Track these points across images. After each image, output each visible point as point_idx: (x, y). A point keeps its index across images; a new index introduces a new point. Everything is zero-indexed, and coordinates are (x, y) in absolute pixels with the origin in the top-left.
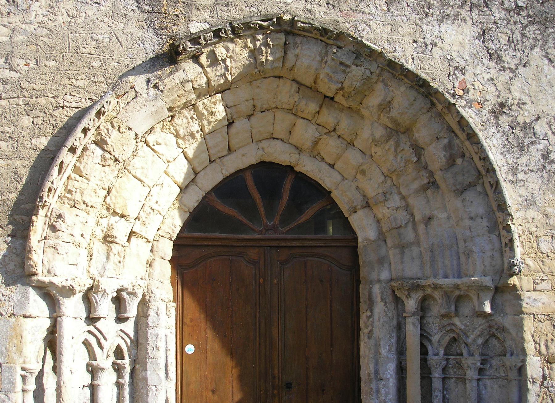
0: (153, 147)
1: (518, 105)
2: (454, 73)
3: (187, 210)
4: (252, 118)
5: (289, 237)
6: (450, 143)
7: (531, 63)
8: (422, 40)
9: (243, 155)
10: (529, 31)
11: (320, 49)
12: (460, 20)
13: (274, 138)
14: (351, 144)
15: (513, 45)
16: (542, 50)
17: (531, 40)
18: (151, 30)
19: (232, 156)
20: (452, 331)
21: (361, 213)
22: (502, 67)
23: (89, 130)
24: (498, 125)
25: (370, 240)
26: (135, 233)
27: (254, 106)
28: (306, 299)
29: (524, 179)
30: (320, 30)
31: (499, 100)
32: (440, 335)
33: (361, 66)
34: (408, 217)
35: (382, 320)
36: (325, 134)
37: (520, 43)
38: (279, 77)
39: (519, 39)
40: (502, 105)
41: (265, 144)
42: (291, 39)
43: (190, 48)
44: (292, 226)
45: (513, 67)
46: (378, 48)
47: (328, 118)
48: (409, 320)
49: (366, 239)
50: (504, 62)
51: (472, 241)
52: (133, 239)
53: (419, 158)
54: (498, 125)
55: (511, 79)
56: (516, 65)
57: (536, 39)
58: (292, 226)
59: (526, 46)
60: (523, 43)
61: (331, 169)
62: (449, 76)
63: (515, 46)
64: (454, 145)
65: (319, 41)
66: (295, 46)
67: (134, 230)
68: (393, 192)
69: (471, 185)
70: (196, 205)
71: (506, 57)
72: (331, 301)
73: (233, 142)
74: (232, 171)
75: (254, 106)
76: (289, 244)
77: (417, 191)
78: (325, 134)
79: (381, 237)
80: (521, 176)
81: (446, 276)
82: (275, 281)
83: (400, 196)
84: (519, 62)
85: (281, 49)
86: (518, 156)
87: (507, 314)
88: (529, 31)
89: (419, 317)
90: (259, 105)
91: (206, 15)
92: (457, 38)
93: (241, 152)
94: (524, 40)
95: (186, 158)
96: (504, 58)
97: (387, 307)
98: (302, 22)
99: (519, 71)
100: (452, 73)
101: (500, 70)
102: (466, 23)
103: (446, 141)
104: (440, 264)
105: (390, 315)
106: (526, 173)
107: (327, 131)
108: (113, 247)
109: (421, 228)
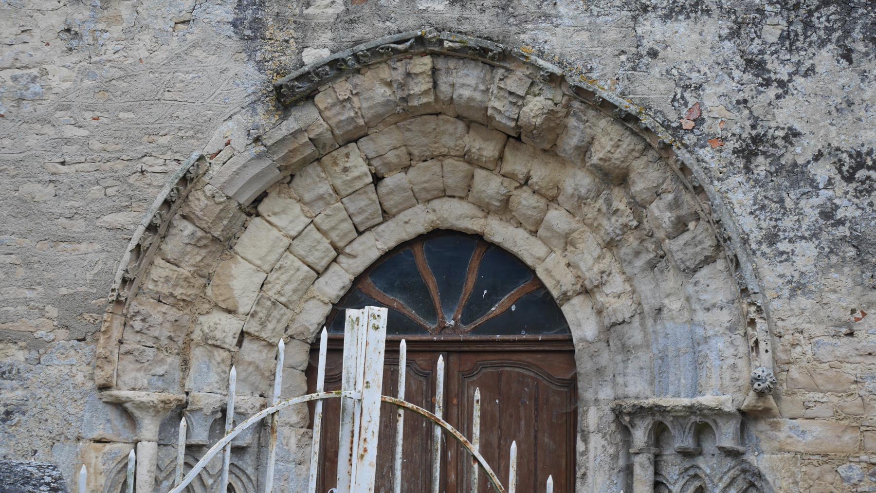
0: (268, 218)
1: (785, 138)
2: (683, 97)
3: (327, 300)
4: (411, 170)
5: (473, 338)
6: (676, 199)
7: (816, 70)
8: (634, 50)
9: (406, 223)
10: (818, 18)
11: (482, 75)
12: (699, 13)
13: (449, 196)
14: (553, 200)
15: (787, 43)
16: (840, 46)
17: (822, 33)
18: (252, 64)
19: (391, 224)
20: (696, 476)
21: (577, 301)
22: (764, 79)
23: (173, 202)
24: (748, 169)
25: (587, 341)
26: (249, 334)
27: (410, 154)
28: (500, 428)
29: (789, 250)
30: (476, 49)
31: (754, 133)
32: (682, 483)
33: (539, 95)
34: (634, 307)
35: (598, 460)
36: (516, 188)
37: (801, 38)
38: (437, 114)
39: (800, 31)
40: (757, 140)
41: (436, 204)
42: (441, 64)
43: (299, 88)
44: (479, 321)
45: (785, 78)
46: (272, 176)
47: (516, 164)
48: (638, 460)
49: (583, 340)
50: (769, 71)
51: (706, 342)
52: (246, 343)
53: (640, 223)
54: (748, 169)
55: (778, 97)
56: (790, 75)
57: (829, 30)
58: (479, 321)
59: (810, 43)
60: (806, 37)
61: (533, 239)
62: (674, 100)
63: (791, 44)
64: (683, 203)
65: (481, 64)
66: (448, 71)
67: (245, 330)
68: (613, 271)
69: (708, 260)
70: (342, 293)
71: (772, 64)
72: (536, 432)
73: (387, 205)
74: (392, 244)
75: (410, 154)
76: (474, 348)
77: (643, 270)
78: (516, 188)
79: (602, 336)
80: (783, 246)
81: (677, 395)
82: (455, 401)
83: (623, 277)
84: (794, 69)
85: (427, 79)
86: (779, 216)
87: (763, 452)
88: (818, 18)
89: (652, 456)
90: (416, 152)
91: (326, 37)
92: (693, 43)
93: (402, 217)
94: (809, 33)
95: (318, 229)
96: (769, 66)
97: (606, 439)
98: (451, 41)
99: (794, 83)
100: (678, 96)
101: (761, 85)
102: (709, 15)
103: (670, 197)
104: (672, 378)
105: (611, 451)
106: (791, 241)
107: (518, 185)
108: (216, 353)
109: (649, 322)
